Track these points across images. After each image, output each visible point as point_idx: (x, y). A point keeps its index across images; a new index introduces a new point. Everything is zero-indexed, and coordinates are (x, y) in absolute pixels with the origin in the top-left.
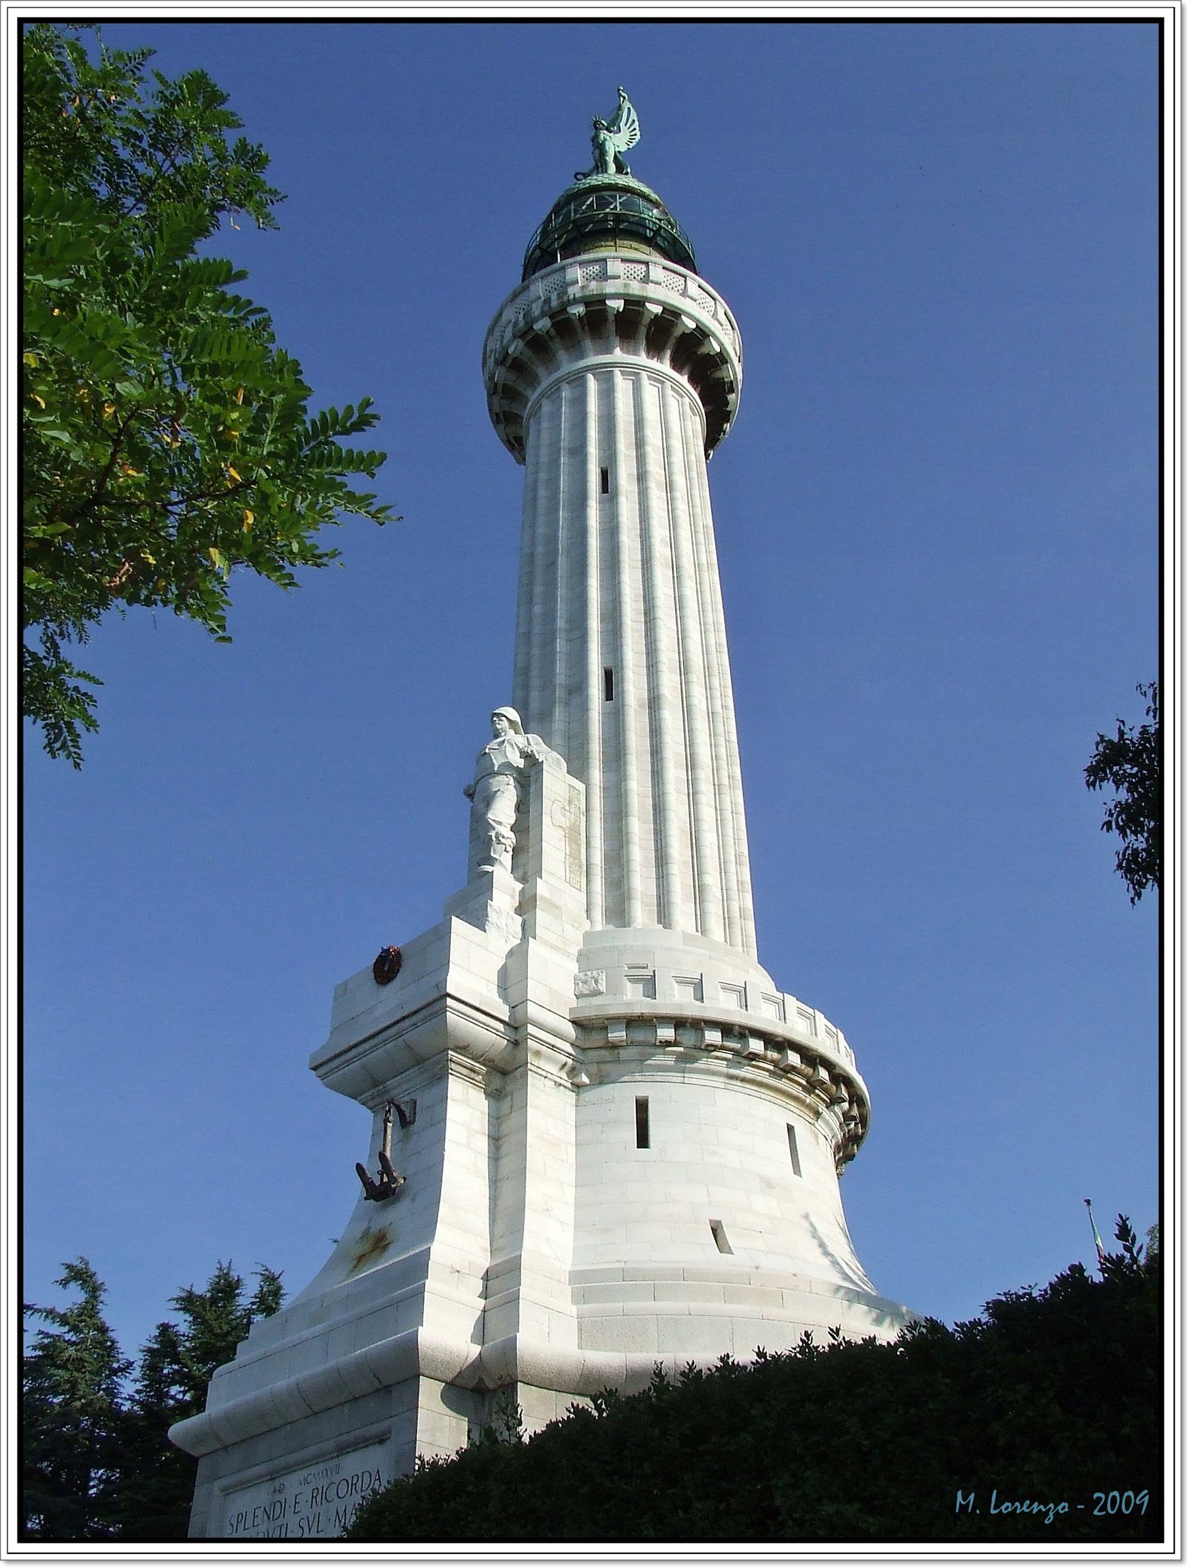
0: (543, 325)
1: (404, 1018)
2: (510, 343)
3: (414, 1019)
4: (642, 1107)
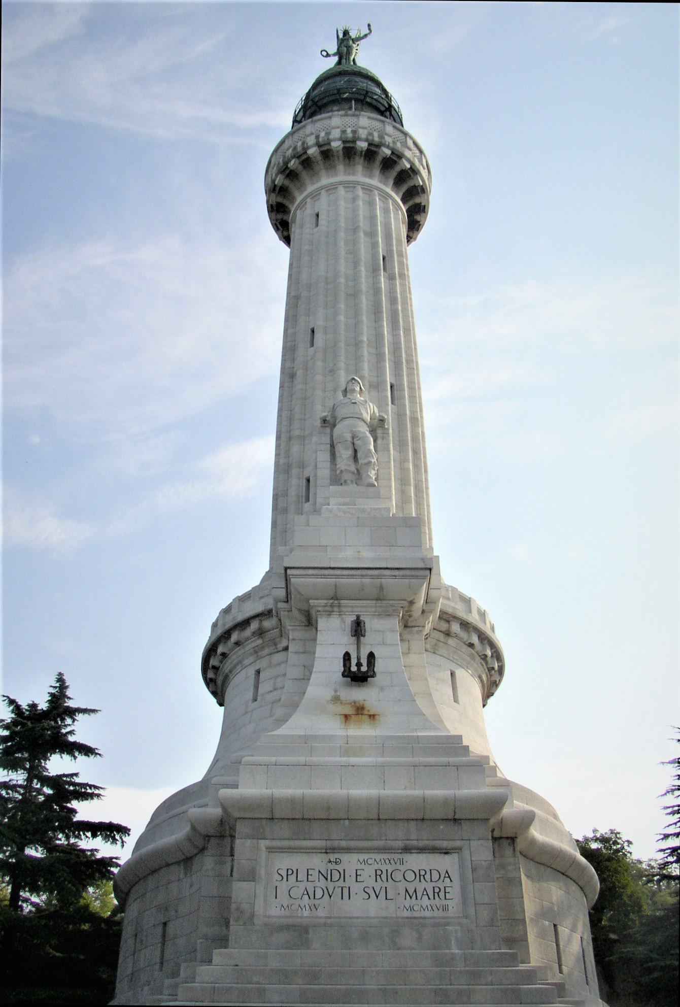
0: (363, 145)
1: (387, 568)
2: (335, 140)
3: (396, 573)
4: (452, 674)
